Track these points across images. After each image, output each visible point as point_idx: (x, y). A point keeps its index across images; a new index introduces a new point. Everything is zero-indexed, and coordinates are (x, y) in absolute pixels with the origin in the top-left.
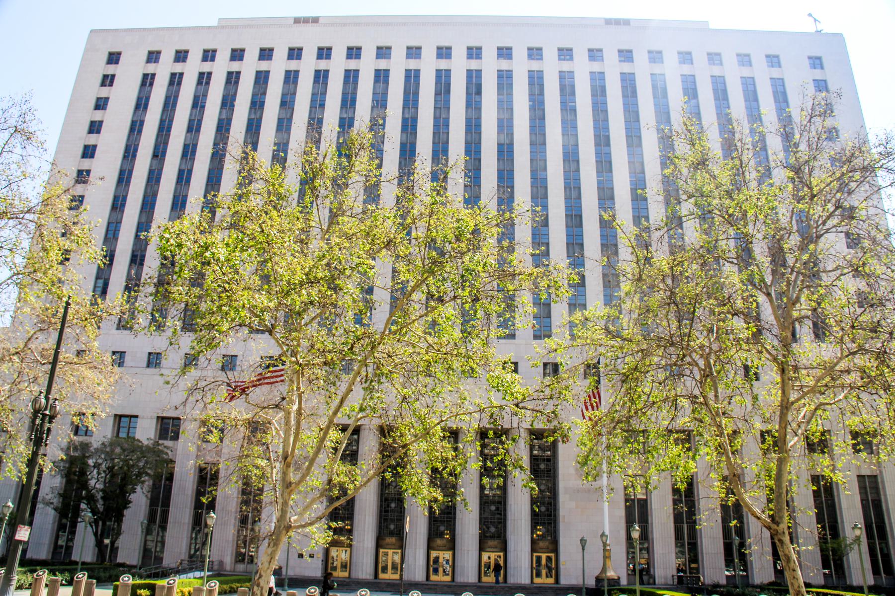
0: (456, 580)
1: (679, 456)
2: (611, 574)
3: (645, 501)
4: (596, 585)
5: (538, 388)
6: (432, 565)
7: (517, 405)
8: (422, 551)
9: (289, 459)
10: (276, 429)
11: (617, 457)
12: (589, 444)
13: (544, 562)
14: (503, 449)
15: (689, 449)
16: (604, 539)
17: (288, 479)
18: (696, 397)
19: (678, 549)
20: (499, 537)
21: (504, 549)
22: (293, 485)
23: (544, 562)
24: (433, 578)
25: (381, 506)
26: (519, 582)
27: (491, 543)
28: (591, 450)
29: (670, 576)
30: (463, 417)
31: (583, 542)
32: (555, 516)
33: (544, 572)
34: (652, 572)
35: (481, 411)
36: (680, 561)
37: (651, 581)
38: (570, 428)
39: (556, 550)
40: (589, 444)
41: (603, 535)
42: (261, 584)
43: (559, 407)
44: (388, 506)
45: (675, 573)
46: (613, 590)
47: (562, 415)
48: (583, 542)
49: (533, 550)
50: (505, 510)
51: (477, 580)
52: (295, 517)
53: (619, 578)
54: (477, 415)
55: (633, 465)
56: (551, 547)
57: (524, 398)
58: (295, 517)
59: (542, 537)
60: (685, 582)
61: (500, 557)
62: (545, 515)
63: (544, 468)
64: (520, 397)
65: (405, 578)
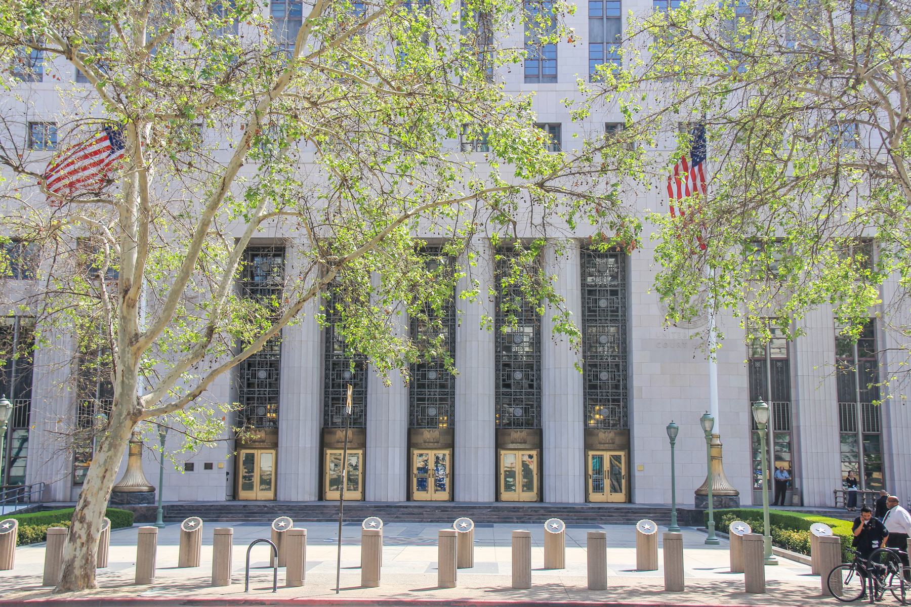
0: (456, 499)
1: (846, 276)
2: (722, 485)
3: (786, 362)
4: (697, 506)
5: (579, 154)
6: (416, 479)
7: (541, 185)
8: (397, 450)
9: (131, 293)
10: (110, 241)
11: (727, 278)
12: (677, 258)
13: (607, 466)
14: (518, 264)
15: (864, 265)
16: (707, 425)
17: (131, 328)
18: (881, 166)
19: (846, 448)
20: (528, 424)
21: (539, 446)
22: (142, 340)
23: (607, 466)
24: (418, 495)
25: (327, 377)
26: (565, 500)
27: (517, 434)
28: (680, 266)
29: (829, 491)
30: (446, 209)
31: (672, 431)
32: (625, 387)
33: (607, 483)
34: (797, 485)
35: (478, 196)
36: (846, 467)
37: (796, 499)
38: (639, 227)
39: (627, 446)
40: (677, 258)
41: (705, 418)
42: (88, 518)
43: (619, 188)
44: (254, 376)
45: (839, 486)
46: (726, 513)
47: (624, 201)
48: (672, 431)
49: (588, 446)
50: (539, 378)
51: (492, 498)
52: (149, 396)
53: (737, 494)
54: (470, 205)
55: (760, 299)
56: (618, 440)
57: (555, 172)
58: (149, 396)
59: (605, 424)
60: (859, 503)
61: (531, 457)
62: (608, 387)
63: (605, 305)
64: (548, 172)
65: (370, 497)
